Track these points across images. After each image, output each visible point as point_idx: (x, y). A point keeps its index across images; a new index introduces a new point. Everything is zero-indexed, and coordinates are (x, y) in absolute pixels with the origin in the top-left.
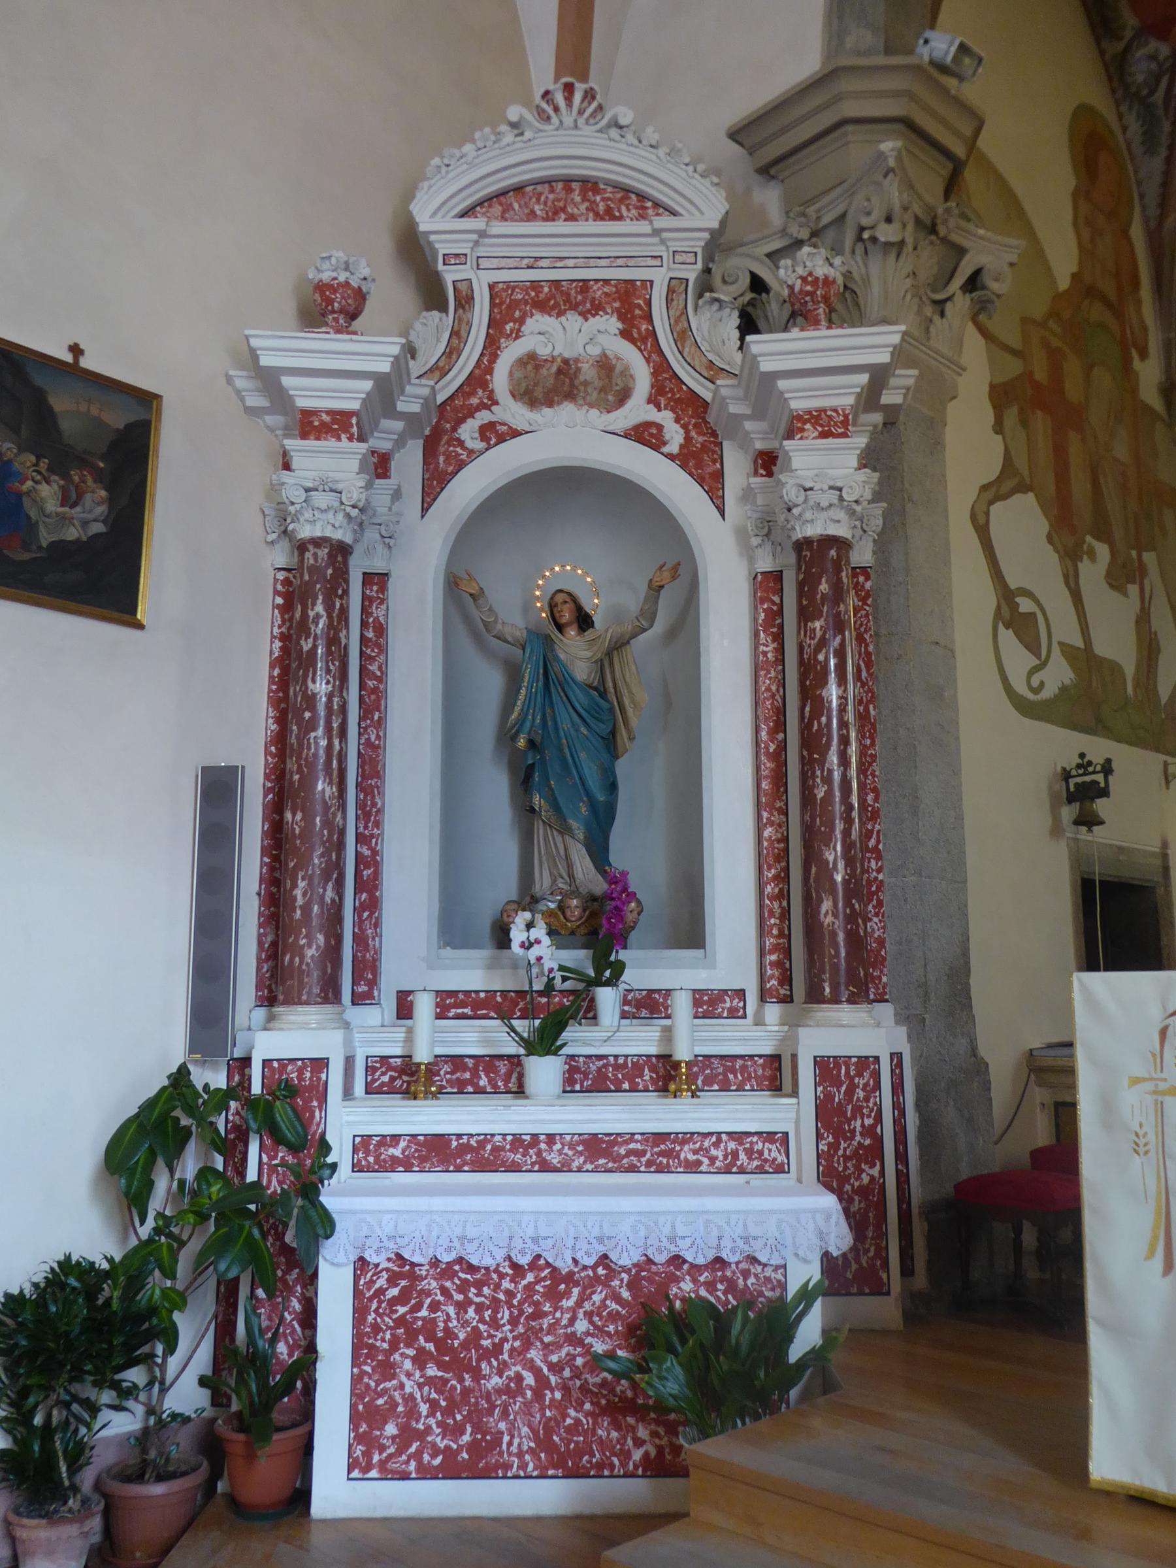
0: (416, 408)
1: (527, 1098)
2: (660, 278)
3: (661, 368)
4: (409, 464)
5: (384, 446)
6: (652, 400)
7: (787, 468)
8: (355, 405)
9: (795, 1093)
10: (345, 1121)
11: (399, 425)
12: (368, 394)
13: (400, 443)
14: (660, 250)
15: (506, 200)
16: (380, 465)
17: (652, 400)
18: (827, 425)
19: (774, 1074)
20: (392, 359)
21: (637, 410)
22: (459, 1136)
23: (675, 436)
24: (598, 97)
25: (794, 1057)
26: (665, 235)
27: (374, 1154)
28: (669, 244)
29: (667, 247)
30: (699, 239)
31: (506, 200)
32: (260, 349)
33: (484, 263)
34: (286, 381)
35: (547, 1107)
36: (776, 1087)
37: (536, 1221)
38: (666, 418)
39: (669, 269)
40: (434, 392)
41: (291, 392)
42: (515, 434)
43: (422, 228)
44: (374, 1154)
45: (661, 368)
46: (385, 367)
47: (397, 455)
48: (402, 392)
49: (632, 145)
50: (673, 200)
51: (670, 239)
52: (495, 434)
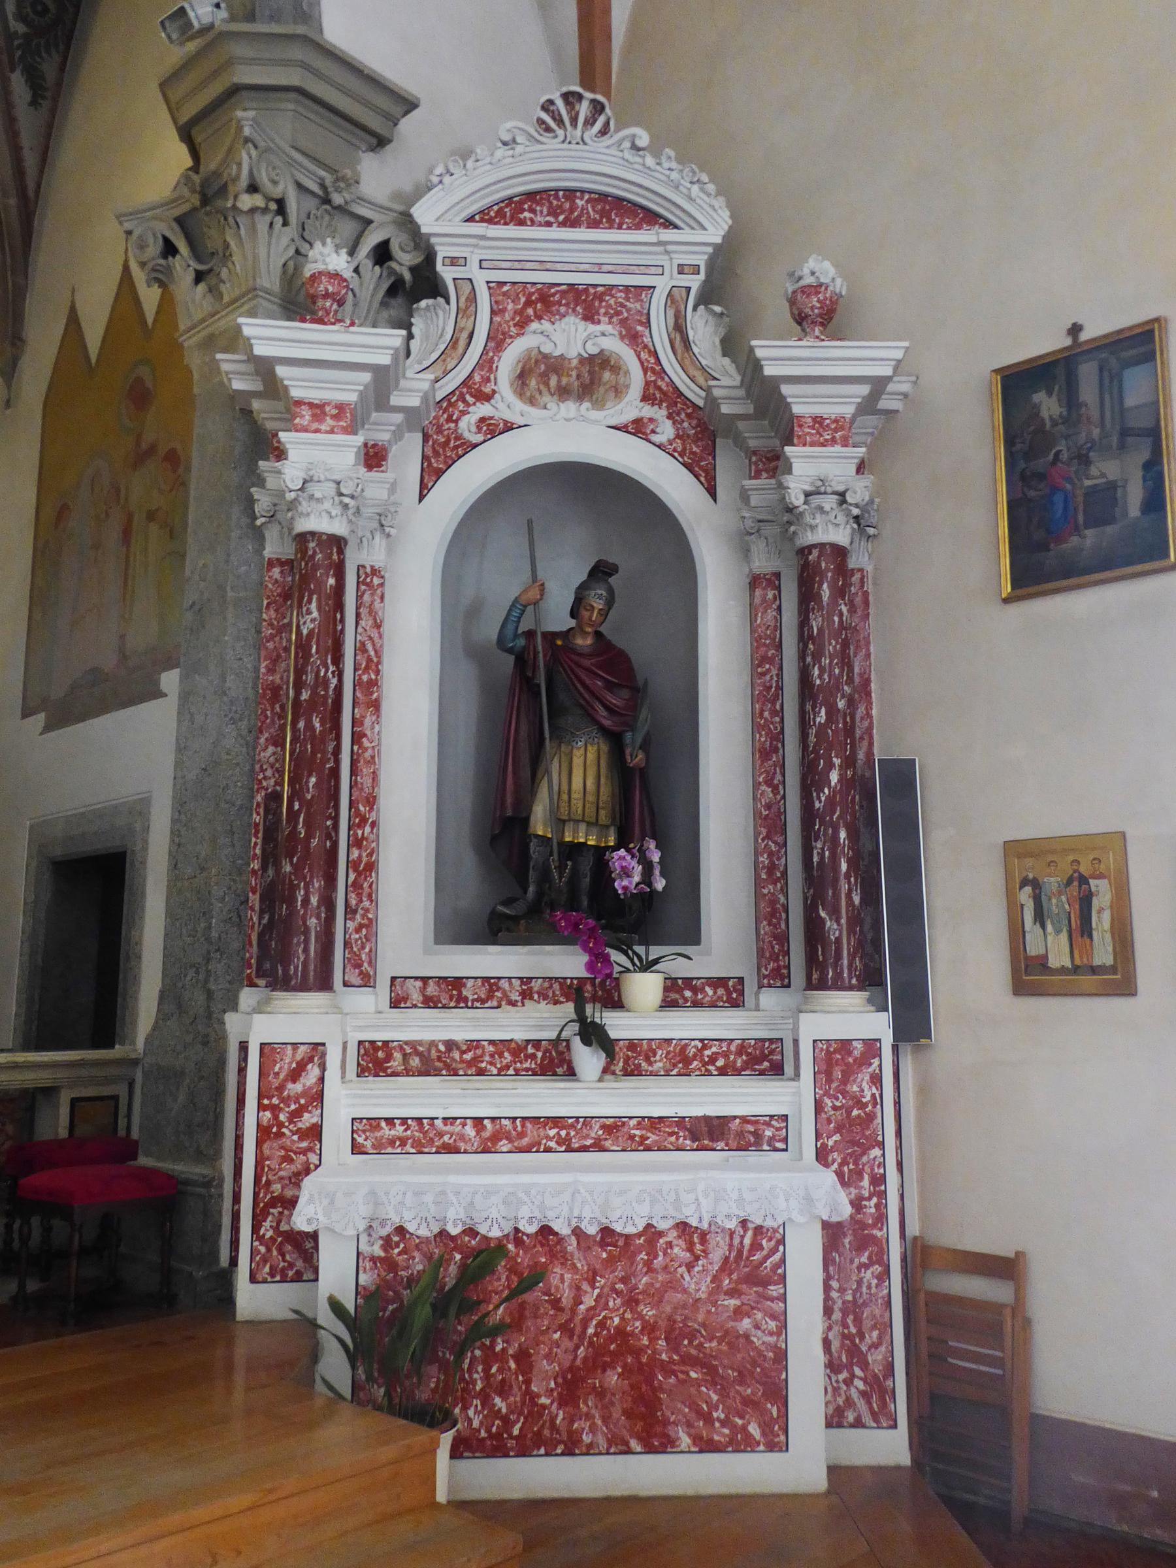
0: (414, 401)
1: (578, 1080)
2: (662, 285)
3: (653, 368)
4: (407, 458)
5: (383, 437)
6: (646, 398)
7: (789, 471)
8: (352, 397)
9: (797, 1075)
10: (346, 1100)
11: (399, 418)
12: (366, 386)
13: (398, 435)
14: (663, 260)
15: (511, 210)
16: (374, 457)
17: (646, 398)
18: (828, 431)
19: (764, 1059)
20: (392, 352)
21: (631, 407)
22: (493, 1119)
23: (666, 431)
24: (552, 97)
25: (796, 1042)
26: (670, 248)
27: (370, 1136)
28: (673, 256)
29: (671, 259)
30: (705, 253)
31: (511, 210)
32: (255, 338)
33: (484, 264)
34: (281, 371)
35: (591, 1094)
36: (777, 1070)
37: (404, 1194)
38: (659, 413)
39: (671, 278)
40: (433, 389)
41: (286, 382)
42: (509, 427)
43: (424, 230)
44: (370, 1136)
45: (653, 368)
46: (385, 359)
47: (394, 448)
48: (397, 385)
49: (649, 168)
50: (575, 180)
51: (675, 252)
52: (493, 429)
